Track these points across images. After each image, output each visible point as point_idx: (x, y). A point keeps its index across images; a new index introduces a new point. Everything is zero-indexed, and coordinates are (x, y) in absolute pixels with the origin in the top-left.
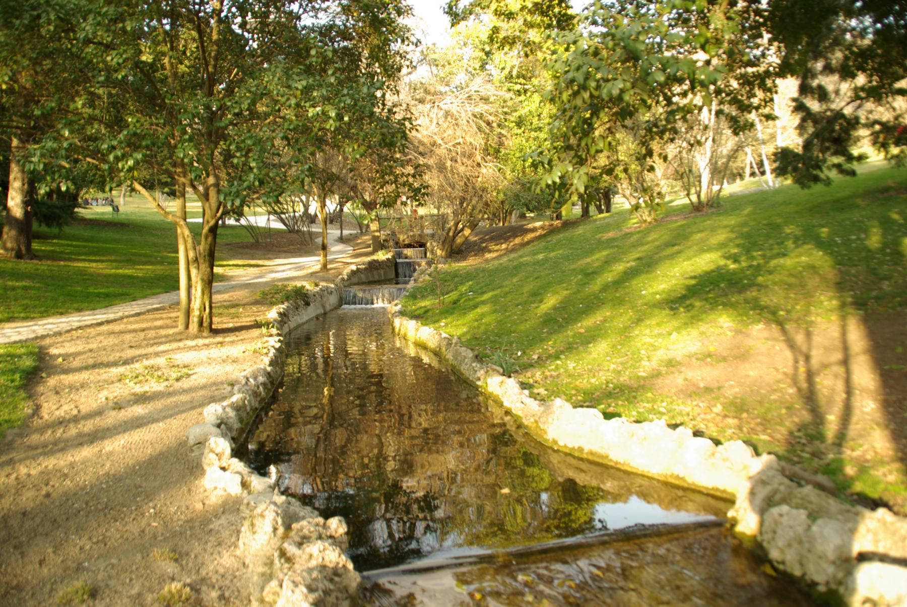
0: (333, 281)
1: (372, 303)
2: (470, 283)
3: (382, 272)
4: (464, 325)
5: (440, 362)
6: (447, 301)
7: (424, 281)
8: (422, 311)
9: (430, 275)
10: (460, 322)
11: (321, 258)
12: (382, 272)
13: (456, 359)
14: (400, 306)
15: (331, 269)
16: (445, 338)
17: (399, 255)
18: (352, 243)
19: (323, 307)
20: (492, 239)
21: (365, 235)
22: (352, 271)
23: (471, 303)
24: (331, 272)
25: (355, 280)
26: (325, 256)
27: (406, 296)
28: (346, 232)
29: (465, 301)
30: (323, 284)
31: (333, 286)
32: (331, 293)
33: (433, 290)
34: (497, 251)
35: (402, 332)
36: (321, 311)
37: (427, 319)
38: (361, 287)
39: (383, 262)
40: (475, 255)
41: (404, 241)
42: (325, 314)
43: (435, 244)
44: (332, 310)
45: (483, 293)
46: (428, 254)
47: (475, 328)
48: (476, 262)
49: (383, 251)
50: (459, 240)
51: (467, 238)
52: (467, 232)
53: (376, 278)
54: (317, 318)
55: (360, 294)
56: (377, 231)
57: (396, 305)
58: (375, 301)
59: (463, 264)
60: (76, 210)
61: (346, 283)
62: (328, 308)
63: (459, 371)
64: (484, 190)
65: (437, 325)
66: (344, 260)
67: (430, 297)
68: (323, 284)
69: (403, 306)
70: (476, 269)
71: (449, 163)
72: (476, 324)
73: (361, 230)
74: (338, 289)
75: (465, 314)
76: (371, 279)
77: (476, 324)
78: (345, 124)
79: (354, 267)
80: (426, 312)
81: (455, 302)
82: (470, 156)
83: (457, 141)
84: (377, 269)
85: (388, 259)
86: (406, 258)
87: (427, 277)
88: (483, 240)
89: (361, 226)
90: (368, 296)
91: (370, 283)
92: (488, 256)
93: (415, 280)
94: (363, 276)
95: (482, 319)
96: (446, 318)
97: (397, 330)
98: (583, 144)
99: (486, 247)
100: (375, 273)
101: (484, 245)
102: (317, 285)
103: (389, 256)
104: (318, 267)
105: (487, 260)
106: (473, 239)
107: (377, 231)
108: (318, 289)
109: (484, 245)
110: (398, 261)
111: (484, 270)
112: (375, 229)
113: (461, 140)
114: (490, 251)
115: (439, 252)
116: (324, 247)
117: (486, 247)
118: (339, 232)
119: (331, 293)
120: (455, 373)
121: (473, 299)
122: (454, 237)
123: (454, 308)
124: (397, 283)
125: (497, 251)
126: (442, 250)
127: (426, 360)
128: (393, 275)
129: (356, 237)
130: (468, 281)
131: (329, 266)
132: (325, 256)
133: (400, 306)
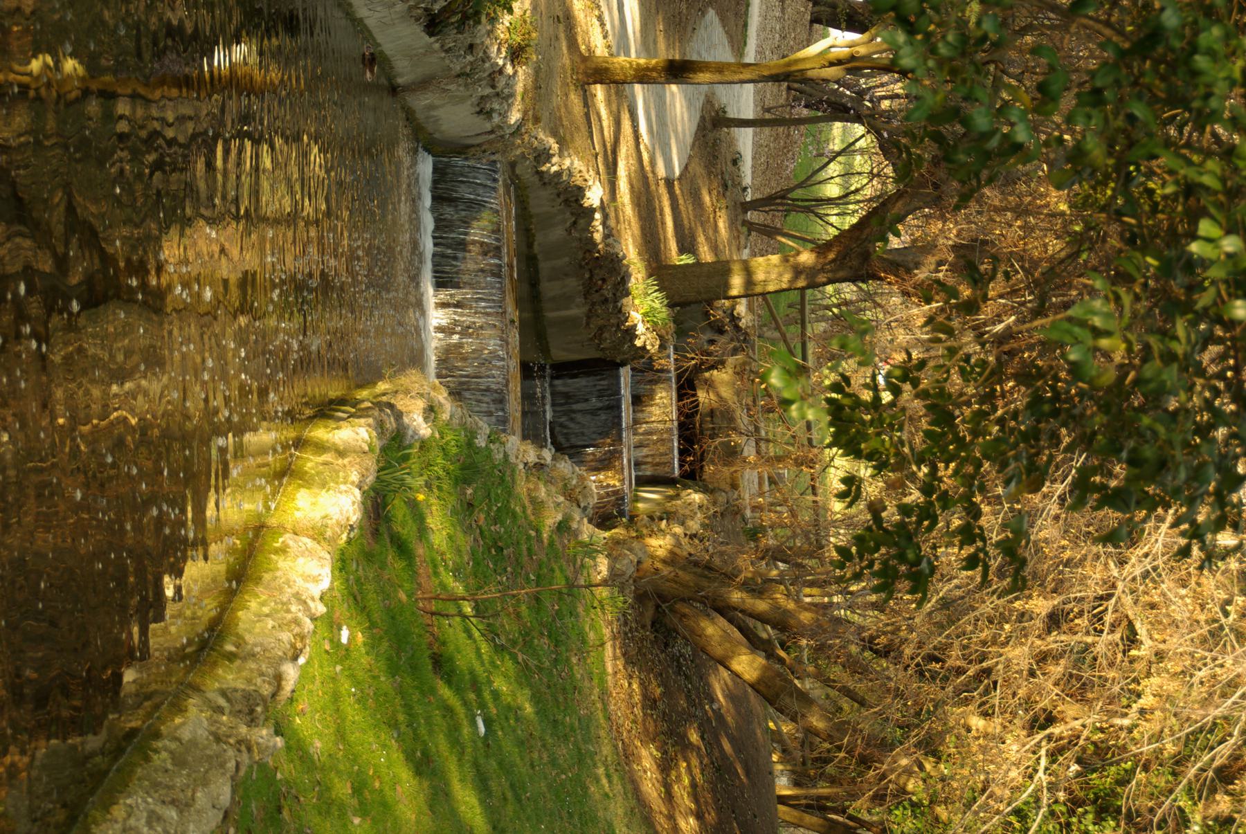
0: (533, 116)
1: (440, 284)
2: (529, 709)
3: (577, 311)
4: (341, 735)
5: (177, 656)
6: (453, 631)
7: (538, 505)
8: (406, 530)
9: (563, 527)
10: (352, 712)
11: (634, 57)
12: (577, 311)
13: (179, 761)
14: (425, 430)
15: (587, 101)
16: (279, 678)
17: (647, 371)
18: (698, 169)
19: (424, 84)
20: (719, 770)
21: (732, 224)
22: (580, 191)
23: (441, 745)
24: (575, 99)
25: (542, 202)
26: (643, 77)
27: (472, 434)
28: (745, 140)
29: (448, 710)
30: (522, 77)
31: (514, 117)
32: (483, 112)
33: (496, 547)
34: (669, 797)
35: (311, 462)
36: (405, 72)
37: (368, 557)
38: (510, 226)
39: (620, 314)
40: (649, 702)
41: (710, 385)
42: (394, 90)
43: (694, 525)
44: (410, 116)
45: (482, 785)
46: (652, 494)
47: (324, 788)
48: (618, 708)
49: (663, 313)
50: (713, 629)
51: (723, 662)
52: (747, 665)
53: (549, 289)
54: (371, 60)
55: (478, 232)
56: (749, 282)
57: (431, 411)
58: (444, 295)
59: (610, 659)
60: (711, 14)
61: (525, 170)
62: (419, 102)
63: (122, 786)
64: (931, 747)
65: (342, 611)
66: (625, 150)
67: (465, 542)
68: (522, 77)
69: (424, 445)
70: (586, 724)
71: (1041, 605)
72: (342, 789)
73: (754, 205)
74: (502, 138)
75: (393, 724)
76: (545, 266)
77: (342, 789)
78: (1219, 302)
79: (594, 195)
80: (402, 548)
81: (441, 663)
82: (1078, 688)
83: (1141, 630)
84: (590, 289)
85: (631, 333)
86: (637, 400)
87: (552, 518)
88: (712, 728)
89: (776, 200)
90: (472, 262)
91: (529, 260)
92: (647, 757)
93: (540, 466)
94: (558, 233)
95: (363, 811)
96: (372, 645)
97: (320, 433)
98: (1136, 191)
99: (685, 746)
100: (573, 284)
101: (694, 737)
102: (516, 54)
103: (645, 337)
104: (597, 42)
105: (627, 757)
106: (719, 685)
107: (749, 282)
108: (500, 59)
109: (694, 737)
110: (625, 374)
111: (582, 759)
112: (760, 276)
113: (1144, 651)
114: (665, 766)
115: (659, 545)
116: (678, 71)
117: (685, 746)
118: (749, 113)
119: (483, 112)
120: (119, 751)
121: (455, 741)
122: (725, 610)
123: (414, 668)
124: (527, 371)
125: (669, 797)
126: (672, 559)
127: (197, 571)
128: (560, 354)
129: (728, 184)
130: (536, 699)
131: (599, 91)
132: (643, 77)
133: (425, 430)
